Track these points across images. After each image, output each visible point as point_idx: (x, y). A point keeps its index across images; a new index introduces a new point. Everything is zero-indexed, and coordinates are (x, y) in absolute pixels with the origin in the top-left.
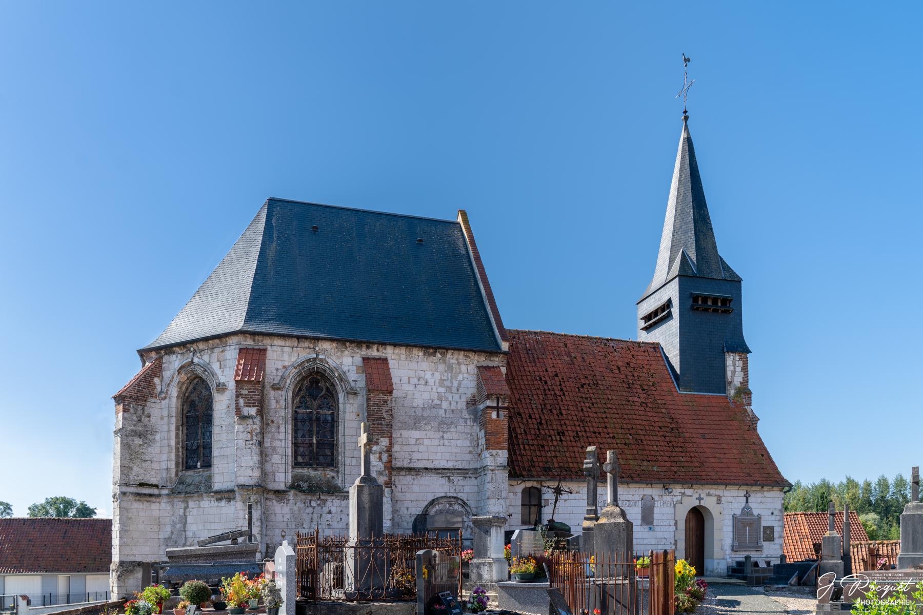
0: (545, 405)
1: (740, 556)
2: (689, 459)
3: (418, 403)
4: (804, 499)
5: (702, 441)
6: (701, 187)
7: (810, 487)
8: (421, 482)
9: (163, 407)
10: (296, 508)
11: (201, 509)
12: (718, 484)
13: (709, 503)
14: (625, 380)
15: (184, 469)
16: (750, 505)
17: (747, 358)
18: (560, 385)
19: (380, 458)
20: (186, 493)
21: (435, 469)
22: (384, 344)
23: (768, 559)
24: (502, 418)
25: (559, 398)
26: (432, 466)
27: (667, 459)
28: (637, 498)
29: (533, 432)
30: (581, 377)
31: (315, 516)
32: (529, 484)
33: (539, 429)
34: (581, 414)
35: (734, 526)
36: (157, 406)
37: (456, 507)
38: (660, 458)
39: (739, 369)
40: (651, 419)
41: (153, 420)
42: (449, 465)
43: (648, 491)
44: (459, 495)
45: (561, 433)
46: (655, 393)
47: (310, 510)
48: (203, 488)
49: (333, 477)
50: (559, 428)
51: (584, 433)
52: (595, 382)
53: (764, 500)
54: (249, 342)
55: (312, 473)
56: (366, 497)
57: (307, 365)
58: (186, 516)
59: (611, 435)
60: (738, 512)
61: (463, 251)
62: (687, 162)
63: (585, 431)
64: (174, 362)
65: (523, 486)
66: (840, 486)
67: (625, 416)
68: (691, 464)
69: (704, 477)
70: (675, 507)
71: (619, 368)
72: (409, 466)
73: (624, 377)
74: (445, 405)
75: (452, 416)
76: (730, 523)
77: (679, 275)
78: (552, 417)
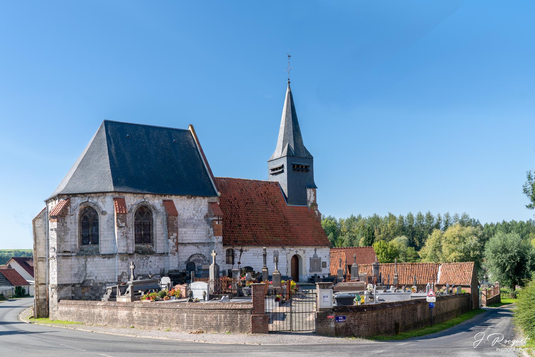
0: (232, 213)
1: (313, 274)
2: (292, 235)
3: (185, 217)
4: (363, 226)
5: (297, 227)
6: (297, 118)
7: (367, 218)
8: (187, 248)
9: (71, 218)
10: (137, 260)
11: (95, 262)
12: (304, 246)
13: (300, 253)
14: (265, 200)
15: (80, 244)
16: (317, 253)
17: (316, 190)
18: (238, 203)
19: (173, 241)
20: (86, 255)
21: (192, 243)
22: (171, 195)
23: (324, 275)
24: (220, 224)
25: (238, 210)
26: (191, 242)
27: (283, 235)
28: (272, 252)
29: (228, 225)
30: (246, 199)
31: (145, 263)
32: (229, 248)
33: (230, 224)
34: (247, 217)
35: (310, 262)
36: (69, 218)
37: (201, 258)
38: (280, 235)
39: (312, 195)
40: (276, 218)
41: (68, 224)
42: (198, 241)
43: (276, 249)
44: (202, 253)
45: (240, 226)
46: (277, 206)
47: (143, 261)
48: (95, 253)
49: (151, 248)
50: (239, 224)
51: (249, 225)
52: (252, 202)
53: (322, 251)
54: (117, 195)
55: (142, 246)
56: (216, 269)
57: (141, 204)
58: (86, 265)
59: (260, 226)
60: (312, 256)
61: (194, 146)
62: (290, 103)
63: (250, 224)
64: (77, 201)
65: (227, 248)
66: (385, 218)
67: (266, 217)
68: (293, 238)
69: (298, 243)
70: (287, 255)
71: (261, 195)
72: (182, 242)
73: (264, 198)
74: (196, 218)
75: (198, 222)
76: (309, 261)
77: (287, 156)
78: (235, 218)
